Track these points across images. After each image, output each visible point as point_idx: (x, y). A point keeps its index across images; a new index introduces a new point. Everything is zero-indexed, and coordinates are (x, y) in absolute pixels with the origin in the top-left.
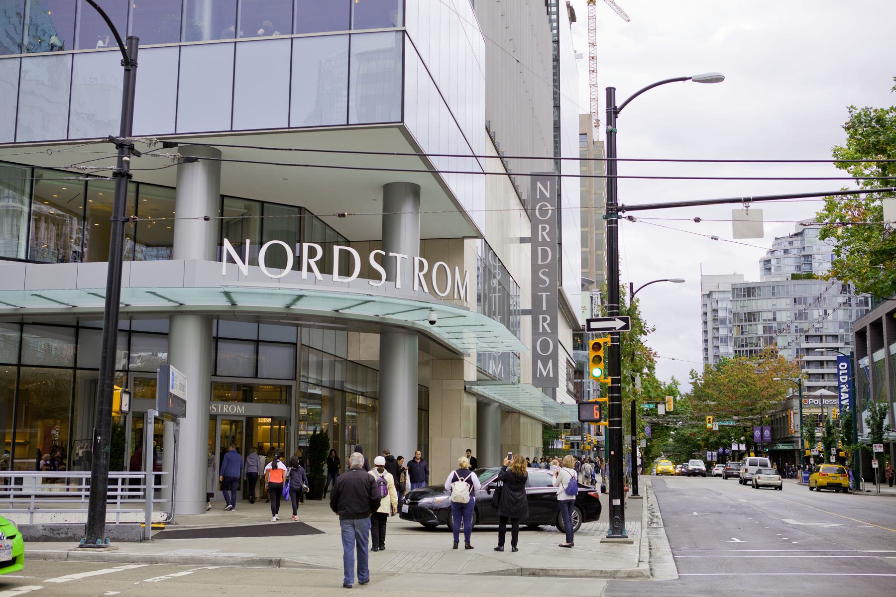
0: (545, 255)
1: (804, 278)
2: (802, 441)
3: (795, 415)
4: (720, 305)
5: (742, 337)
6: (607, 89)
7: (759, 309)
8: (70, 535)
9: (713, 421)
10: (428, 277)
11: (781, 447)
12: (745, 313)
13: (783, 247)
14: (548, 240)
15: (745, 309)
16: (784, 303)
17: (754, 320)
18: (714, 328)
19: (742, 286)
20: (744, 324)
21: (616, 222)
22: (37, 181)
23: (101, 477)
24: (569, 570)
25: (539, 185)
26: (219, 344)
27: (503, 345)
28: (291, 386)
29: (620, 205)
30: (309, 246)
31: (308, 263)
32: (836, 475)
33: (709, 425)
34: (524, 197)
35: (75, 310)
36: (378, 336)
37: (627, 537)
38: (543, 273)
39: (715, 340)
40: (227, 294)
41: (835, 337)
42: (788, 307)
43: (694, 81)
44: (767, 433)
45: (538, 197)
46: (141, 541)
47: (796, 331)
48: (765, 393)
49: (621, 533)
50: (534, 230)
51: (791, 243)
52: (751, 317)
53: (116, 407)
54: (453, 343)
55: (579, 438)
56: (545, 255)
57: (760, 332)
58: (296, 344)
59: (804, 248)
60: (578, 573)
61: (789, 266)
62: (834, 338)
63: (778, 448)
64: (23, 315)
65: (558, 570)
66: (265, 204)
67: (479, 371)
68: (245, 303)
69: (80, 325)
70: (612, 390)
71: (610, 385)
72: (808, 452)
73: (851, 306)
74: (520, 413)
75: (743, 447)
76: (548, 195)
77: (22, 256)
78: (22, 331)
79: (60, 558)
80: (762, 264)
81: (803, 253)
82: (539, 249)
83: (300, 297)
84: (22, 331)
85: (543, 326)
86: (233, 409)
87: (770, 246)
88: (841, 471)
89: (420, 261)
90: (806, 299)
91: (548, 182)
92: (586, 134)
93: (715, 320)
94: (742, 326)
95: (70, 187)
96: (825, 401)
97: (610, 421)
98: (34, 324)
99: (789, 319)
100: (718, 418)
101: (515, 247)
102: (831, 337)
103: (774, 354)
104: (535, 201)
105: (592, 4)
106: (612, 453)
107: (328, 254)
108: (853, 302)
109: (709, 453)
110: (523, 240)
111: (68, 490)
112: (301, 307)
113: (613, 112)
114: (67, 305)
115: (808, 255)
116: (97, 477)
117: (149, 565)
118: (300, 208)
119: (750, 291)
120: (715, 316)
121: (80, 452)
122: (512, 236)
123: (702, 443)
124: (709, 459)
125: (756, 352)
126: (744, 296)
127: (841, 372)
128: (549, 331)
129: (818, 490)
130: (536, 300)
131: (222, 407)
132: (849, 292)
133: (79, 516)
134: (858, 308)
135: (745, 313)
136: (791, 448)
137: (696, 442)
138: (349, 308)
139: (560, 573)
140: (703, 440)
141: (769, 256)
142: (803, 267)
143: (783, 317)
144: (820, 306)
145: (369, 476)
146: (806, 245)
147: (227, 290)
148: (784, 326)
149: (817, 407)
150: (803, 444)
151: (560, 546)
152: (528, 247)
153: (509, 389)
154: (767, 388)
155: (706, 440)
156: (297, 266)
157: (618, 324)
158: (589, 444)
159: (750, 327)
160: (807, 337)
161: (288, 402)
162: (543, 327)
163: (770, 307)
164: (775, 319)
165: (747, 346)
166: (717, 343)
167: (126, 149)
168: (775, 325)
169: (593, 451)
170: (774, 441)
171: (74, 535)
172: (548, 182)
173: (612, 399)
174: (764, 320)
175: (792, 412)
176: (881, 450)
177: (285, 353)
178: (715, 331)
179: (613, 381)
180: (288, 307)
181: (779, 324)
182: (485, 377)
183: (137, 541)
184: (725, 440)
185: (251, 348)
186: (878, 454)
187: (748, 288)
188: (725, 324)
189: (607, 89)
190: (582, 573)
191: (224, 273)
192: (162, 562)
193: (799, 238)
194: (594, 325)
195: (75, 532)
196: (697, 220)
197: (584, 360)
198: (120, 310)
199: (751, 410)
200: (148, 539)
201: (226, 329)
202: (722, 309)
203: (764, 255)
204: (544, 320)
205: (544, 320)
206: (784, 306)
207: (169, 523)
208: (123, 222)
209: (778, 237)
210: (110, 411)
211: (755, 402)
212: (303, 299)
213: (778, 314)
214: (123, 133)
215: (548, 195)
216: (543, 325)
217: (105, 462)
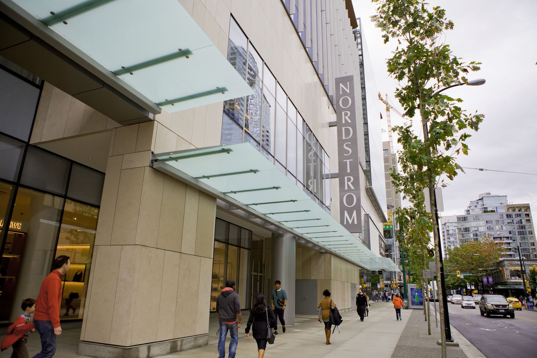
0: (347, 132)
1: (490, 212)
3: (507, 270)
4: (450, 228)
5: (463, 238)
9: (460, 274)
11: (500, 287)
12: (464, 228)
13: (474, 205)
14: (350, 121)
15: (464, 226)
16: (482, 223)
17: (469, 231)
18: (448, 238)
19: (462, 217)
20: (464, 233)
25: (341, 85)
27: (366, 255)
33: (458, 276)
34: (330, 94)
38: (347, 146)
39: (449, 243)
41: (507, 238)
42: (484, 225)
44: (491, 279)
45: (341, 93)
50: (339, 117)
52: (467, 230)
55: (389, 282)
56: (347, 132)
57: (471, 236)
59: (483, 205)
62: (507, 238)
63: (499, 288)
73: (514, 224)
74: (331, 253)
75: (473, 288)
76: (348, 91)
80: (466, 212)
81: (483, 207)
82: (343, 128)
85: (348, 184)
90: (492, 221)
91: (348, 83)
92: (388, 150)
93: (448, 234)
94: (463, 234)
99: (485, 230)
100: (462, 271)
101: (327, 129)
102: (505, 238)
105: (388, 111)
108: (515, 222)
109: (452, 291)
110: (331, 125)
115: (486, 208)
119: (464, 219)
120: (448, 233)
123: (451, 286)
126: (463, 221)
128: (353, 188)
130: (342, 165)
132: (512, 218)
134: (518, 225)
135: (464, 228)
136: (506, 288)
137: (448, 286)
140: (452, 284)
141: (469, 209)
143: (482, 229)
144: (499, 224)
146: (484, 204)
148: (482, 234)
149: (517, 265)
150: (525, 285)
153: (331, 239)
155: (453, 284)
158: (396, 284)
159: (467, 234)
160: (494, 238)
162: (348, 185)
163: (475, 225)
166: (449, 244)
168: (478, 233)
169: (398, 288)
172: (348, 83)
175: (504, 269)
178: (448, 239)
184: (463, 284)
188: (452, 236)
193: (481, 201)
197: (391, 243)
202: (451, 230)
204: (349, 180)
205: (349, 180)
206: (482, 225)
216: (348, 184)
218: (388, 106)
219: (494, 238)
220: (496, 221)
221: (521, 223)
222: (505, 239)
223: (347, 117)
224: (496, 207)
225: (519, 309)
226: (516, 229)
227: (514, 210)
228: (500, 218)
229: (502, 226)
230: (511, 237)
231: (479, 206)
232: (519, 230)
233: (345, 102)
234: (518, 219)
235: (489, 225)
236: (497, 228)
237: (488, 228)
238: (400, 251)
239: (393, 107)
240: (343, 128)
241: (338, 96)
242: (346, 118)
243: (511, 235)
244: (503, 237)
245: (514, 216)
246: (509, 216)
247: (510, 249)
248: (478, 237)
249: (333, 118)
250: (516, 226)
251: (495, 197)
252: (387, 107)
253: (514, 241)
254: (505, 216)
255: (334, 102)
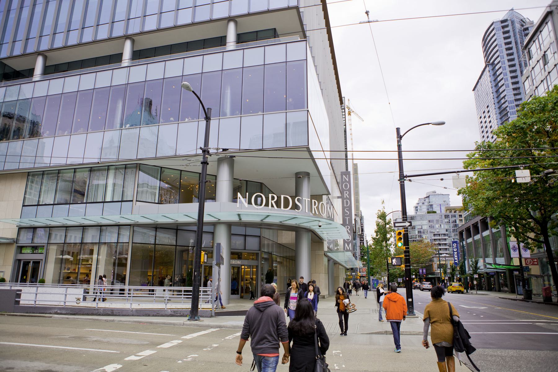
2: (441, 274)
6: (397, 128)
7: (416, 224)
8: (182, 314)
10: (318, 208)
11: (430, 276)
14: (348, 197)
16: (425, 222)
17: (414, 229)
21: (404, 182)
22: (163, 173)
23: (196, 290)
24: (408, 332)
26: (84, 242)
28: (258, 253)
29: (405, 175)
30: (272, 196)
31: (271, 202)
32: (459, 287)
35: (177, 222)
36: (295, 232)
37: (415, 315)
40: (239, 215)
41: (445, 234)
42: (427, 224)
43: (432, 124)
44: (424, 271)
46: (210, 317)
47: (430, 233)
48: (423, 256)
49: (413, 313)
51: (425, 200)
53: (202, 260)
54: (321, 235)
56: (347, 202)
57: (417, 233)
58: (260, 236)
60: (412, 333)
61: (424, 209)
64: (157, 224)
65: (403, 332)
66: (248, 182)
67: (328, 248)
68: (245, 219)
69: (178, 228)
70: (405, 252)
71: (405, 250)
72: (443, 278)
76: (347, 180)
77: (157, 201)
78: (156, 231)
79: (180, 325)
80: (415, 208)
82: (345, 200)
83: (268, 216)
84: (156, 231)
86: (236, 262)
87: (417, 202)
88: (460, 285)
89: (314, 201)
90: (433, 220)
95: (174, 175)
96: (447, 259)
97: (405, 265)
98: (161, 228)
103: (421, 241)
104: (342, 183)
106: (407, 279)
107: (279, 198)
108: (451, 221)
109: (399, 279)
110: (338, 197)
111: (173, 295)
112: (268, 220)
113: (400, 137)
114: (175, 220)
116: (195, 290)
117: (219, 329)
118: (261, 183)
121: (177, 279)
122: (335, 196)
124: (399, 281)
125: (415, 241)
127: (454, 247)
129: (452, 293)
131: (232, 261)
132: (449, 218)
133: (187, 305)
134: (453, 224)
138: (286, 221)
139: (404, 333)
141: (417, 205)
142: (430, 209)
143: (425, 227)
145: (272, 286)
146: (430, 201)
147: (239, 213)
150: (441, 275)
151: (398, 130)
152: (340, 200)
154: (424, 254)
155: (399, 274)
156: (267, 205)
157: (407, 224)
161: (257, 259)
163: (420, 224)
164: (422, 228)
165: (412, 238)
167: (206, 153)
168: (422, 230)
170: (427, 274)
171: (183, 314)
173: (405, 256)
174: (418, 229)
176: (477, 277)
177: (257, 240)
179: (406, 248)
180: (262, 220)
181: (424, 230)
182: (330, 250)
183: (209, 317)
185: (242, 238)
186: (476, 278)
187: (412, 217)
189: (397, 128)
190: (414, 333)
191: (238, 206)
192: (224, 327)
193: (428, 198)
194: (397, 225)
195: (184, 313)
196: (442, 180)
198: (204, 222)
199: (418, 262)
200: (213, 316)
201: (235, 230)
203: (415, 205)
207: (217, 309)
208: (205, 182)
209: (420, 198)
210: (200, 262)
211: (419, 260)
212: (270, 217)
213: (423, 226)
214: (205, 146)
215: (347, 180)
217: (198, 283)
218: (350, 110)
219: (434, 235)
220: (436, 220)
221: (456, 222)
222: (443, 235)
223: (347, 195)
224: (440, 205)
225: (25, 277)
226: (451, 227)
227: (451, 212)
228: (440, 218)
229: (441, 225)
230: (447, 234)
231: (426, 204)
232: (454, 228)
233: (346, 186)
234: (454, 219)
235: (431, 223)
236: (437, 226)
237: (430, 226)
238: (361, 250)
239: (354, 111)
240: (345, 200)
241: (342, 183)
242: (346, 195)
243: (447, 233)
244: (441, 234)
245: (450, 216)
246: (447, 216)
247: (446, 244)
248: (422, 234)
249: (339, 195)
250: (452, 225)
251: (440, 196)
252: (349, 112)
253: (449, 237)
254: (443, 217)
255: (340, 185)
